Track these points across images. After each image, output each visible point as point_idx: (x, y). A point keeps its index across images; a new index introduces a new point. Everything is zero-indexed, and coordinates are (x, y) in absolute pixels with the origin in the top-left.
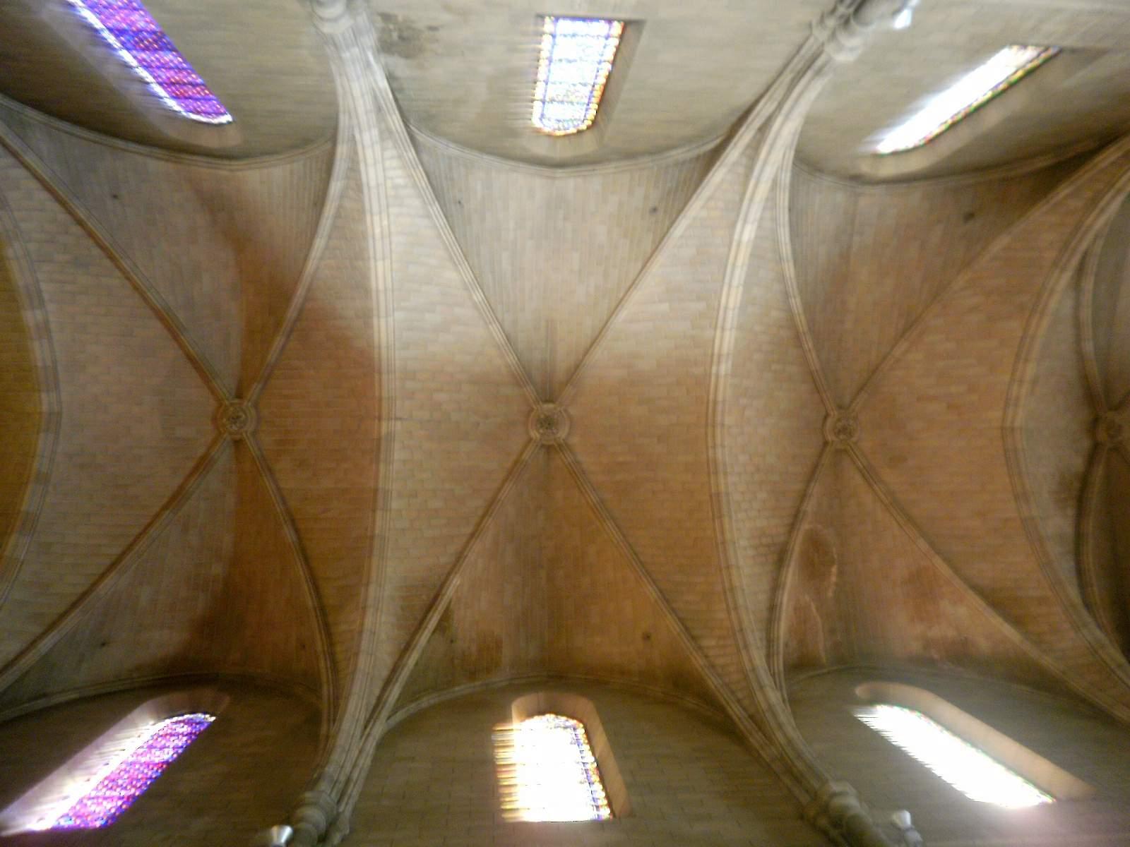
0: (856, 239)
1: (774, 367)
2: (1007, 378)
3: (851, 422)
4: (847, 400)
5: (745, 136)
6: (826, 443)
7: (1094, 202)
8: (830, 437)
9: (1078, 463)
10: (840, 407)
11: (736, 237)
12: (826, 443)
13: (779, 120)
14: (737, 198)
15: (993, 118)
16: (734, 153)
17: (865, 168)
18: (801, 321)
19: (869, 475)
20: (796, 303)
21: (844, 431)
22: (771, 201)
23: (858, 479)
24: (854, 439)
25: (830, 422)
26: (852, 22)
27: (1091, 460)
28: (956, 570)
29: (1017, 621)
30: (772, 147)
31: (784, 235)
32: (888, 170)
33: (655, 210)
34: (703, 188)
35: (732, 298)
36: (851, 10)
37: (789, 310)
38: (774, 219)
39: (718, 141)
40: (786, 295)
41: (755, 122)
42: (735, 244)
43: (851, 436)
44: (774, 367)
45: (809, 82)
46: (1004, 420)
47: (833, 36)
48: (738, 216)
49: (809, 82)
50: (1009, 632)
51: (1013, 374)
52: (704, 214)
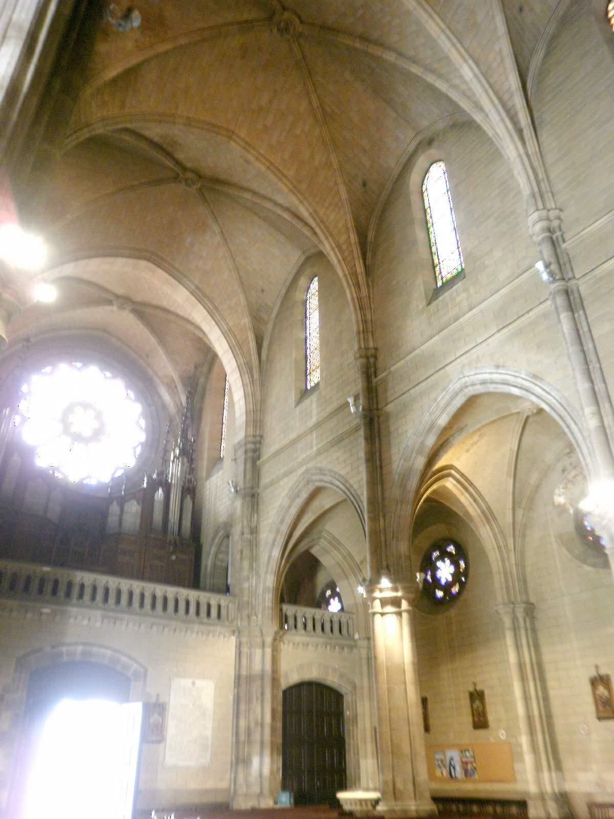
0: (394, 115)
1: (360, 12)
2: (262, 151)
3: (288, 37)
4: (302, 41)
5: (524, 119)
6: (284, 9)
7: (339, 246)
8: (286, 15)
9: (180, 156)
10: (301, 35)
11: (470, 61)
12: (284, 9)
13: (522, 150)
14: (492, 80)
15: (420, 235)
16: (518, 102)
17: (433, 152)
18: (377, 51)
19: (246, 26)
20: (390, 57)
21: (284, 30)
22: (469, 95)
23: (246, 16)
24: (275, 31)
25: (297, 22)
26: (548, 234)
27: (177, 162)
28: (158, 56)
29: (114, 81)
30: (508, 131)
31: (441, 86)
32: (421, 161)
33: (521, 10)
34: (513, 62)
35: (433, 27)
36: (554, 237)
37: (390, 48)
38: (455, 87)
39: (529, 94)
40: (400, 54)
41: (528, 133)
42: (467, 56)
43: (278, 30)
44: (360, 12)
45: (532, 187)
46: (238, 136)
47: (548, 219)
48: (482, 73)
49: (532, 187)
50: (111, 74)
51: (262, 155)
52: (497, 48)
